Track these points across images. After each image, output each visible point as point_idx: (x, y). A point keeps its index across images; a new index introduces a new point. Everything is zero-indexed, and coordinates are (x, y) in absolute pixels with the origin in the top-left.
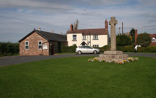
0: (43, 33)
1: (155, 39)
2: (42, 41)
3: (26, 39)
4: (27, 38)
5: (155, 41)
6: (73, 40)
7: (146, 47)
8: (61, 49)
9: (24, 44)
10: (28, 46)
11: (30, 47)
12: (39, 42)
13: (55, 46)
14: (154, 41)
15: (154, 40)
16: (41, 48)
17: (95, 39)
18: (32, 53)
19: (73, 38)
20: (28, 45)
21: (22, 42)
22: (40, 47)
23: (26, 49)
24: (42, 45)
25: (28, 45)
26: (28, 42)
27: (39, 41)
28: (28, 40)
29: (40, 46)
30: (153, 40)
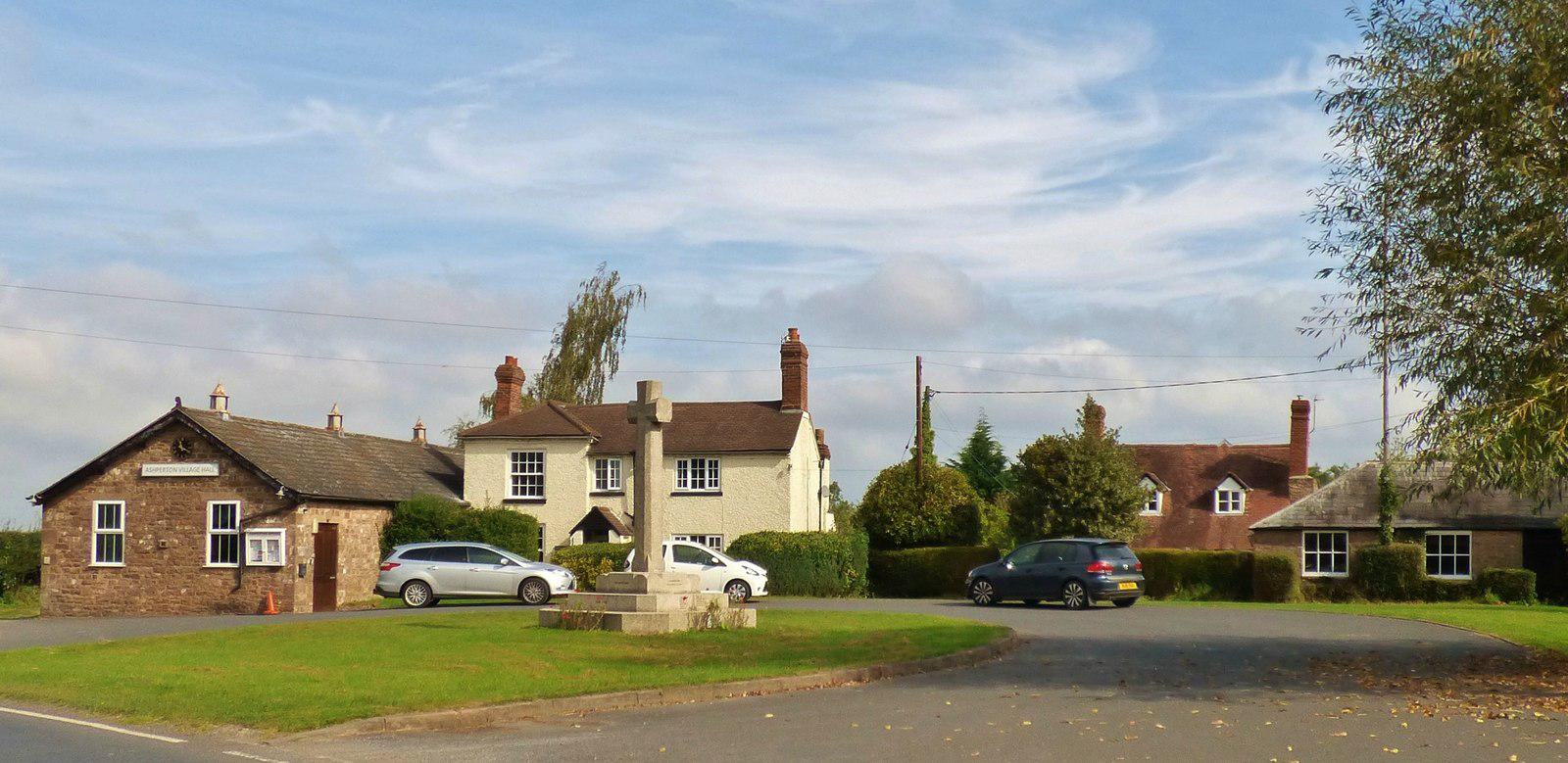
0: (156, 428)
1: (1236, 488)
2: (238, 503)
3: (106, 478)
4: (116, 471)
5: (1235, 506)
6: (676, 489)
7: (362, 692)
8: (341, 560)
9: (81, 519)
10: (119, 536)
11: (137, 549)
12: (216, 507)
13: (350, 540)
14: (1231, 512)
15: (1231, 501)
16: (233, 560)
17: (689, 488)
18: (151, 592)
19: (540, 468)
20: (122, 530)
21: (66, 503)
22: (229, 548)
23: (99, 558)
24: (236, 531)
25: (122, 530)
26: (123, 503)
27: (96, 504)
28: (117, 489)
29: (110, 536)
30: (1223, 495)
